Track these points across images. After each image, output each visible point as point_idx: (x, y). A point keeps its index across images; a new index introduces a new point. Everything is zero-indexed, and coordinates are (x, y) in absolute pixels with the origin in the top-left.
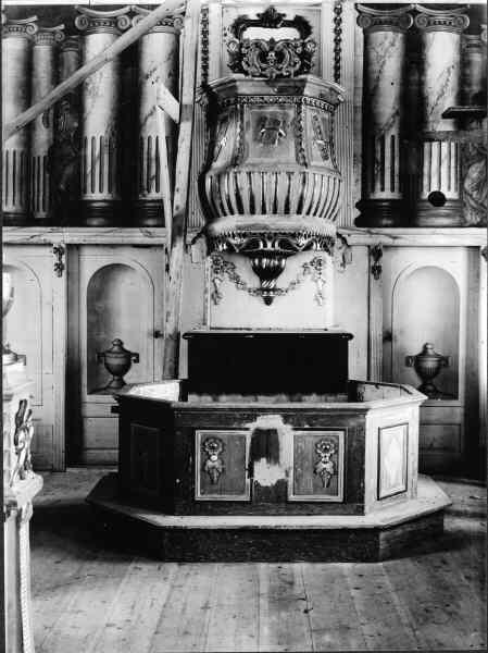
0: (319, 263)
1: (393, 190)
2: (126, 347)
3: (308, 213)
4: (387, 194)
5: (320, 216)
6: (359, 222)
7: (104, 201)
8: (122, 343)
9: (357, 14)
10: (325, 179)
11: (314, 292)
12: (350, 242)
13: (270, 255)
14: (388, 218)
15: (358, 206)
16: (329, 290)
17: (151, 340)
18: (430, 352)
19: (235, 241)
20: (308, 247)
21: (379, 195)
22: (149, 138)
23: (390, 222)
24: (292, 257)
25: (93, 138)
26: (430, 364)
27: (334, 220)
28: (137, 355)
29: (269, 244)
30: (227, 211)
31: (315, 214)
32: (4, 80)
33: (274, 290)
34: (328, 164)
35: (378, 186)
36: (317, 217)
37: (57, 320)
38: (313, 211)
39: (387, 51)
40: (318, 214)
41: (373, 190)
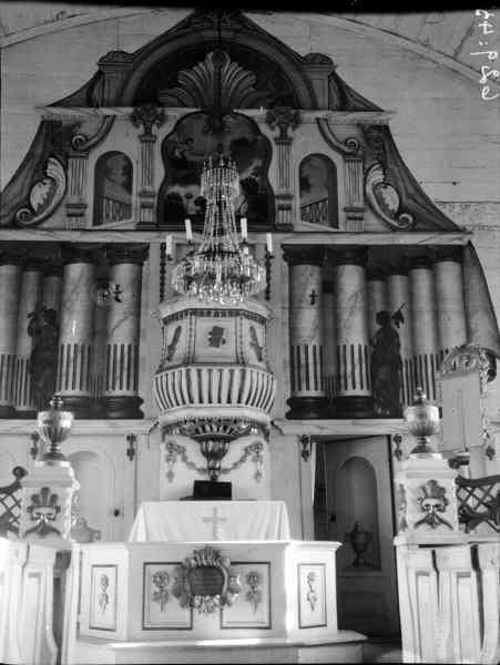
0: (258, 446)
1: (316, 389)
2: (89, 526)
3: (247, 403)
4: (313, 393)
5: (252, 404)
6: (289, 416)
7: (77, 397)
8: (85, 523)
9: (460, 503)
10: (260, 376)
11: (253, 472)
12: (284, 431)
13: (215, 439)
14: (315, 412)
15: (289, 402)
16: (264, 468)
17: (113, 517)
18: (359, 529)
19: (186, 426)
20: (247, 433)
21: (305, 393)
22: (116, 346)
23: (314, 415)
24: (235, 442)
25: (69, 346)
26: (361, 539)
27: (269, 411)
28: (99, 532)
29: (215, 429)
30: (174, 403)
31: (252, 404)
32: (259, 661)
33: (219, 469)
34: (262, 365)
35: (304, 385)
36: (249, 406)
37: (77, 572)
38: (250, 402)
39: (307, 279)
40: (250, 402)
41: (300, 389)
